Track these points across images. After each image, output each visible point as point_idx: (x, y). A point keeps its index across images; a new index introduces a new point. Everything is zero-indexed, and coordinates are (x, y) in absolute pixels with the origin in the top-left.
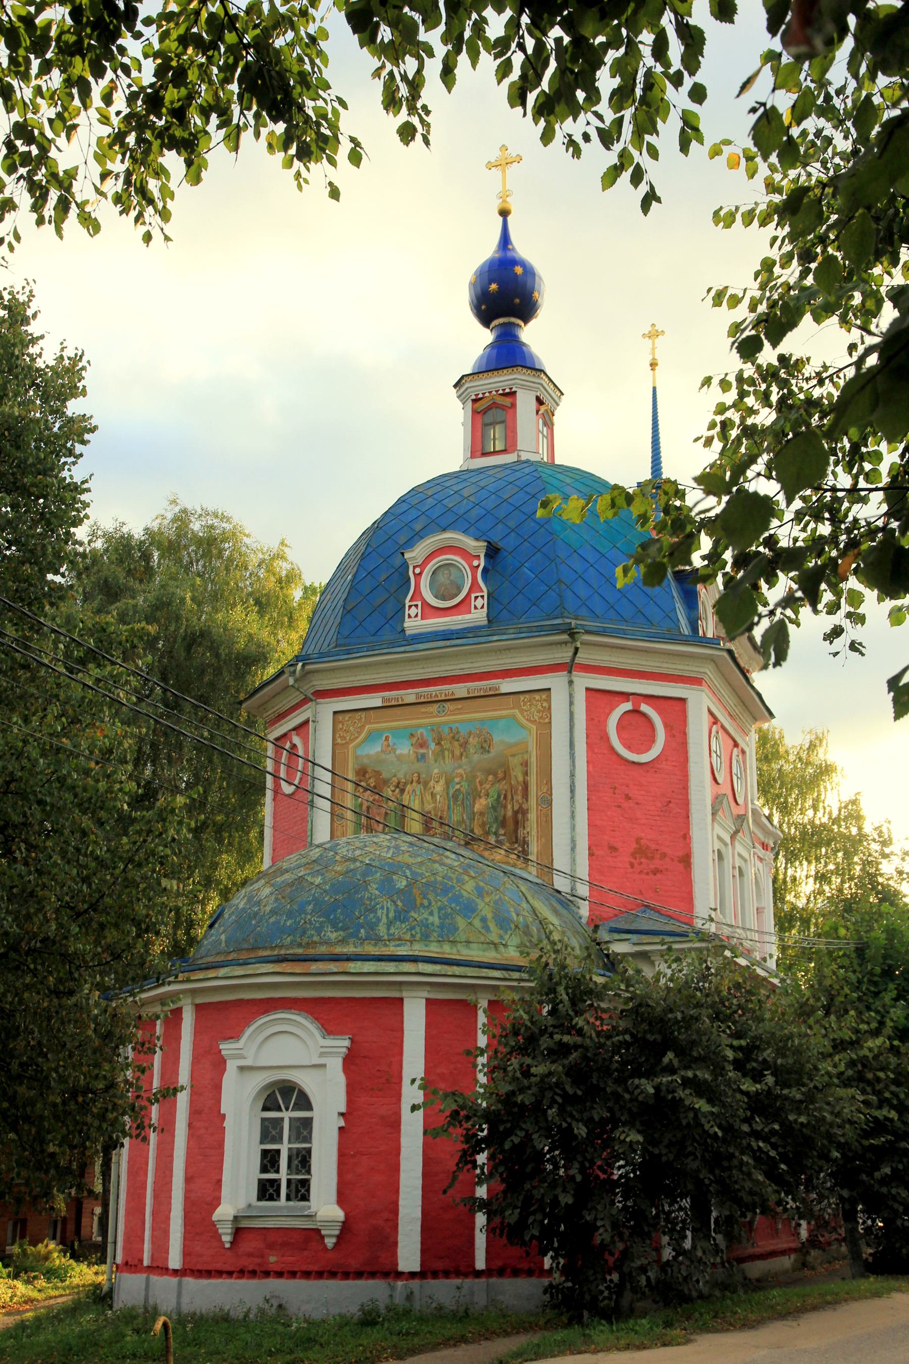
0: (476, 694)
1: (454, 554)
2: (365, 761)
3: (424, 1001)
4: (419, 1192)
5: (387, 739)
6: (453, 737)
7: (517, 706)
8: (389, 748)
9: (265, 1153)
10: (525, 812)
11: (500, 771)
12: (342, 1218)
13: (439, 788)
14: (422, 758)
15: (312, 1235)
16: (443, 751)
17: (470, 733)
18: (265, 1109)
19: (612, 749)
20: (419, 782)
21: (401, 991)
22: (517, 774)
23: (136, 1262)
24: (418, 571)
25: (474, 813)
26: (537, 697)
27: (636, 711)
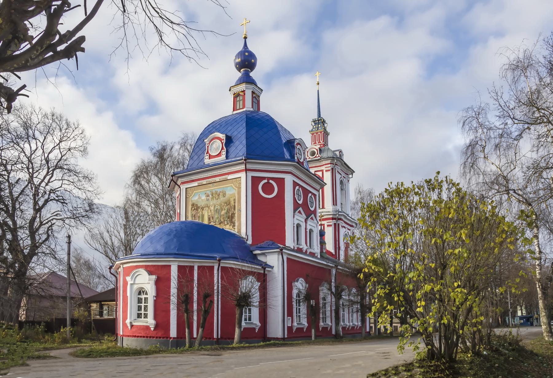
2: (194, 202)
7: (233, 183)
8: (200, 198)
11: (228, 203)
13: (212, 208)
14: (208, 200)
15: (148, 328)
22: (232, 203)
27: (268, 183)
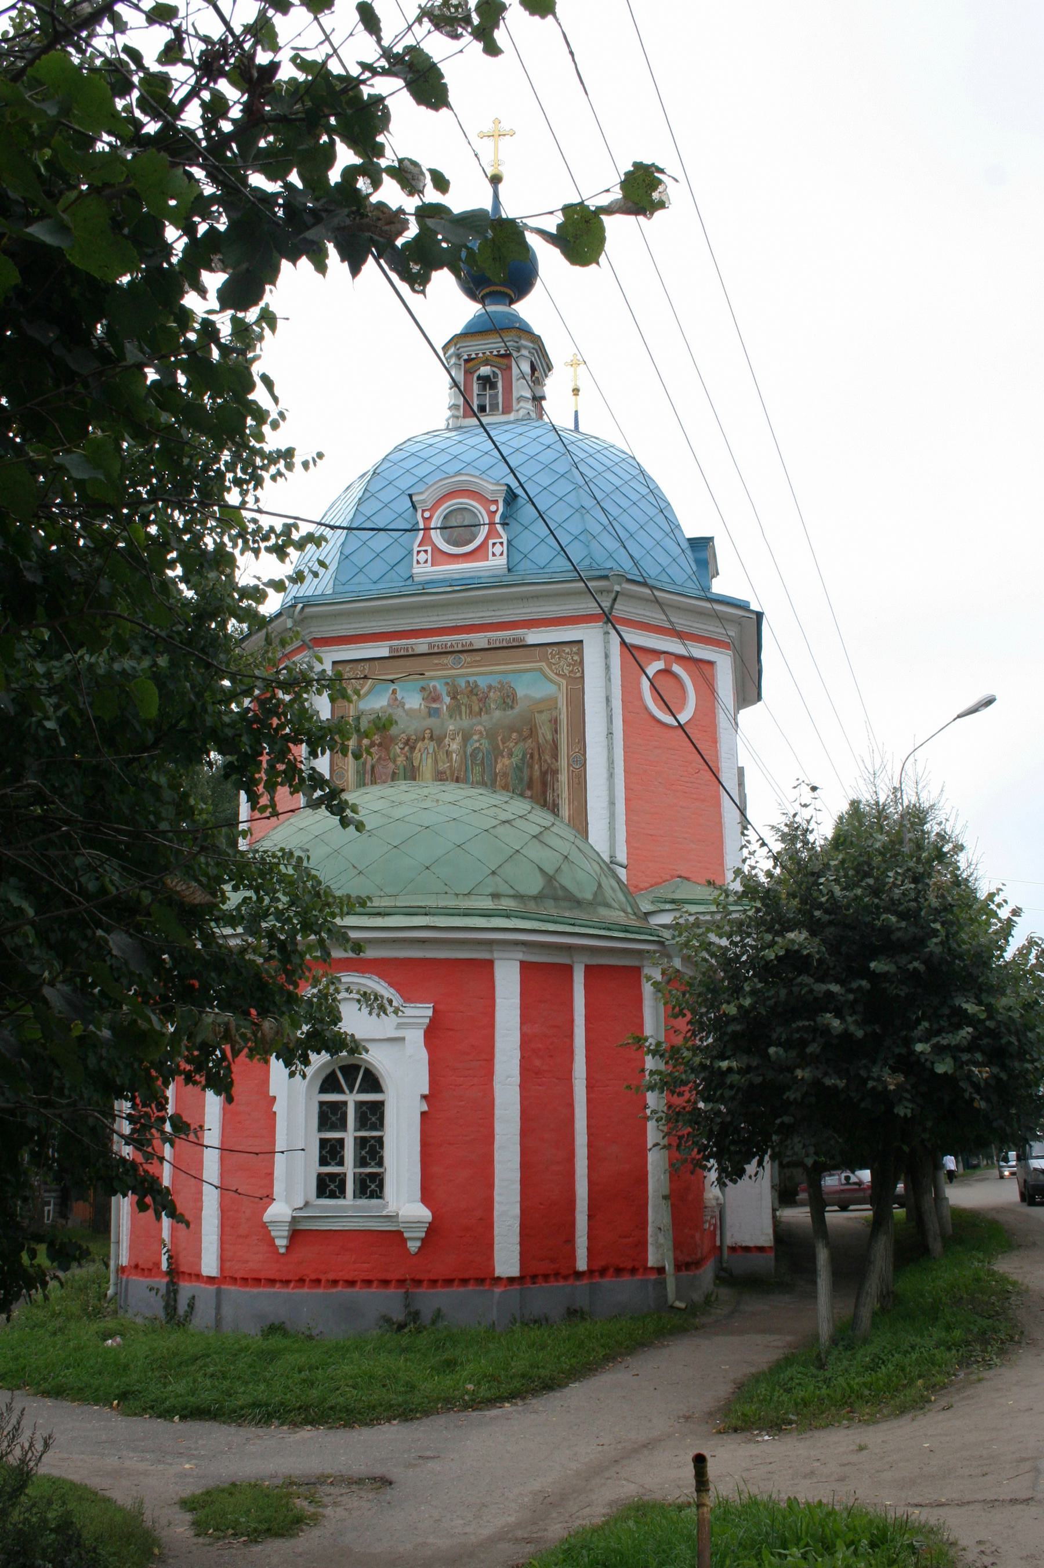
0: (498, 645)
1: (468, 497)
3: (518, 963)
4: (518, 1186)
5: (394, 692)
6: (471, 691)
7: (544, 658)
9: (323, 1142)
10: (555, 772)
11: (528, 729)
12: (430, 1219)
13: (454, 746)
14: (432, 713)
16: (459, 706)
17: (490, 687)
18: (323, 1090)
19: (646, 708)
20: (431, 738)
21: (491, 951)
22: (545, 732)
23: (150, 1265)
24: (427, 514)
25: (496, 775)
26: (567, 650)
27: (667, 672)
